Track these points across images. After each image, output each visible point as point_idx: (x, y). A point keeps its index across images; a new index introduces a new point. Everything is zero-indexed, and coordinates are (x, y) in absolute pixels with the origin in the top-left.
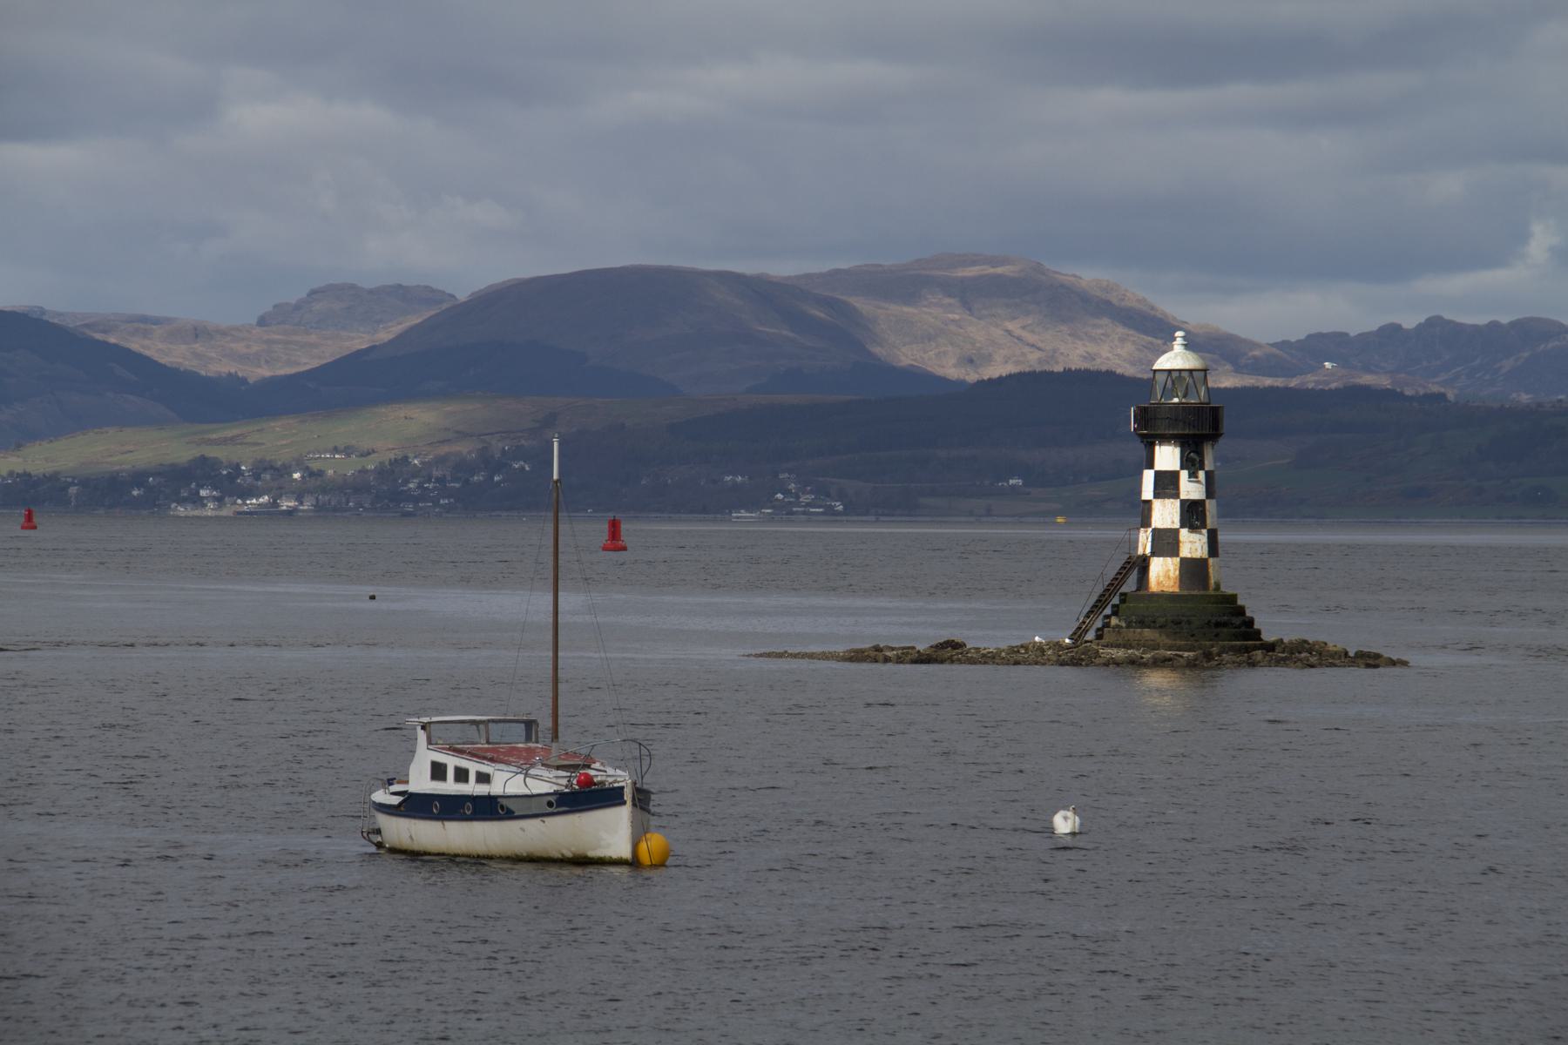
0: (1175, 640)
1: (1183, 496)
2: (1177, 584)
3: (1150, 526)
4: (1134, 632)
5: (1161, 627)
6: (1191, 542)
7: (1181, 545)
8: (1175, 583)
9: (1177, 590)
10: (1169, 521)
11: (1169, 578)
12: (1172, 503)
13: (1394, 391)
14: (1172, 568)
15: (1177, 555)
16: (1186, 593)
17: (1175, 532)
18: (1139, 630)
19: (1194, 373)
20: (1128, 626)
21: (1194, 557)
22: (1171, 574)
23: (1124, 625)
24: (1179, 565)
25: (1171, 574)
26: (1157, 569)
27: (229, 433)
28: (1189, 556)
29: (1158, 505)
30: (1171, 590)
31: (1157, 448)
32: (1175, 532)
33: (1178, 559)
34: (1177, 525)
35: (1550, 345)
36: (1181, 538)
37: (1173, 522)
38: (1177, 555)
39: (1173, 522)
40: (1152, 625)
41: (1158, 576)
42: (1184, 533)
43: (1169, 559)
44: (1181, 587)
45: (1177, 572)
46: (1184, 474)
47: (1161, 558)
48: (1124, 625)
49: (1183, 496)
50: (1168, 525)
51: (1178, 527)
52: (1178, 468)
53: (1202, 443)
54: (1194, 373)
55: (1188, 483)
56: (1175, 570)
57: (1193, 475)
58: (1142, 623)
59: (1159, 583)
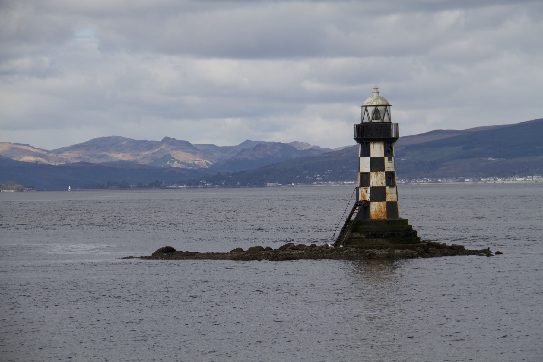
0: (394, 244)
1: (386, 170)
2: (386, 215)
3: (369, 185)
4: (372, 240)
5: (385, 237)
6: (390, 193)
7: (387, 195)
8: (385, 214)
9: (386, 218)
10: (380, 183)
11: (382, 212)
12: (381, 174)
13: (55, 165)
14: (383, 207)
15: (385, 200)
16: (390, 219)
17: (383, 189)
18: (375, 239)
19: (368, 108)
20: (367, 237)
21: (392, 201)
22: (383, 210)
23: (363, 237)
24: (386, 205)
25: (383, 210)
26: (374, 208)
27: (139, 192)
28: (390, 200)
29: (373, 175)
30: (383, 218)
31: (372, 146)
32: (383, 189)
33: (386, 202)
34: (384, 185)
35: (157, 150)
36: (387, 192)
37: (382, 183)
38: (385, 200)
39: (382, 183)
40: (381, 236)
41: (376, 211)
42: (387, 188)
43: (381, 202)
44: (388, 216)
45: (386, 209)
46: (386, 159)
47: (377, 202)
48: (363, 237)
49: (386, 170)
50: (379, 185)
51: (385, 186)
52: (383, 156)
53: (370, 143)
54: (368, 108)
55: (388, 163)
56: (384, 208)
57: (390, 159)
58: (375, 236)
59: (376, 215)
